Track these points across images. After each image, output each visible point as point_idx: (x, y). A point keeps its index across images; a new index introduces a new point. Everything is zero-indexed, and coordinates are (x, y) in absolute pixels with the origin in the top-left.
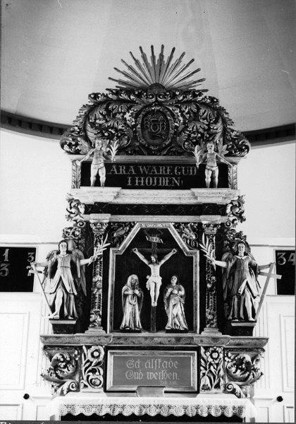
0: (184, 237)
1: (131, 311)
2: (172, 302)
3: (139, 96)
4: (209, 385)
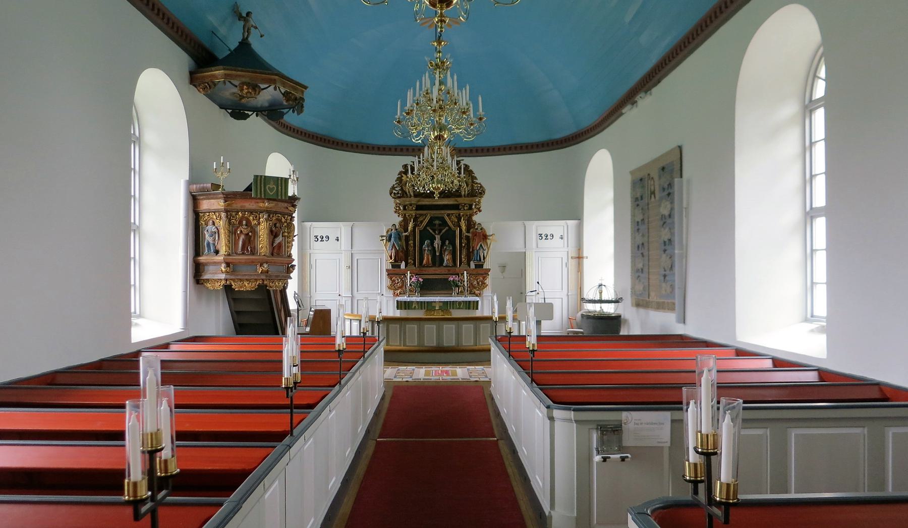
1: (427, 258)
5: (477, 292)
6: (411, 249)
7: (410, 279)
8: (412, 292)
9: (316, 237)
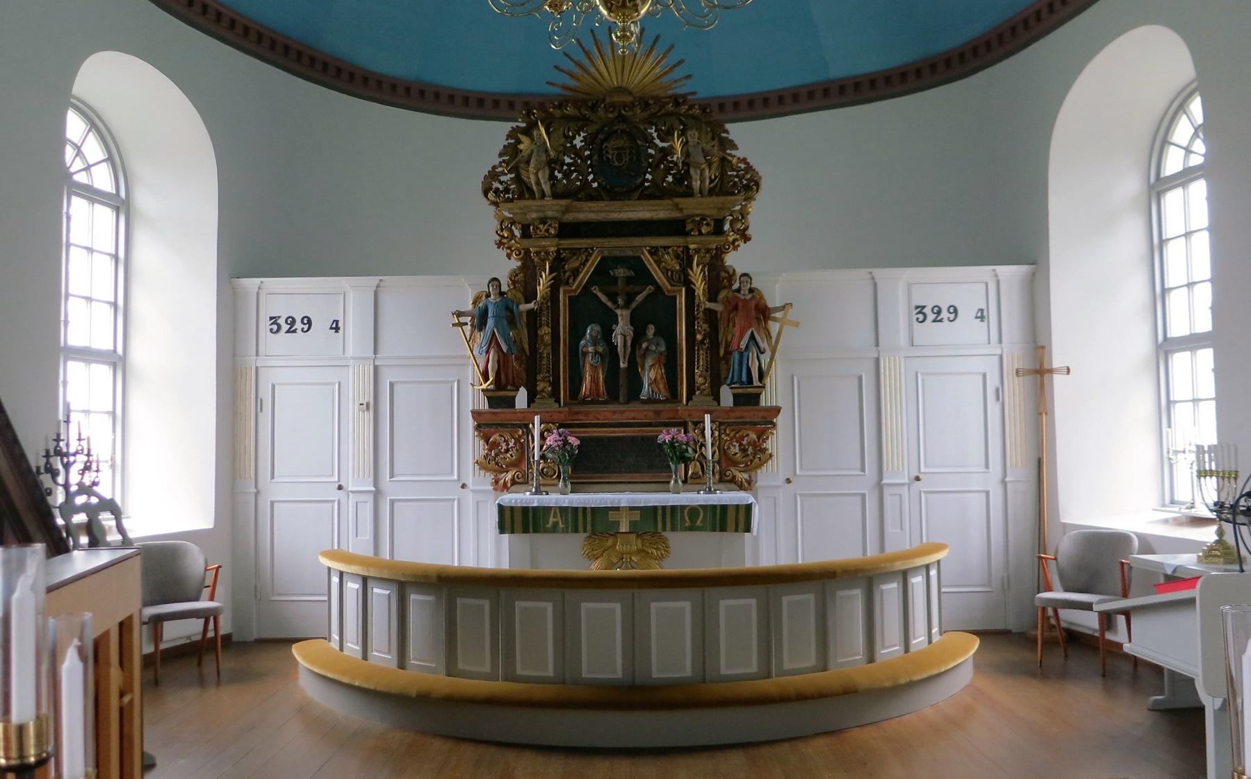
6: (545, 351)
7: (541, 439)
8: (547, 478)
9: (274, 320)
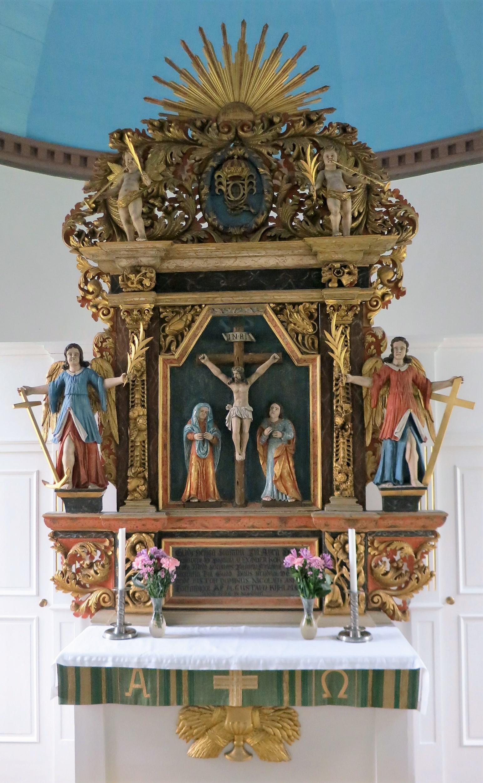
0: (293, 330)
1: (200, 469)
2: (273, 453)
3: (203, 128)
4: (340, 601)
5: (394, 602)
6: (139, 438)
7: (132, 560)
